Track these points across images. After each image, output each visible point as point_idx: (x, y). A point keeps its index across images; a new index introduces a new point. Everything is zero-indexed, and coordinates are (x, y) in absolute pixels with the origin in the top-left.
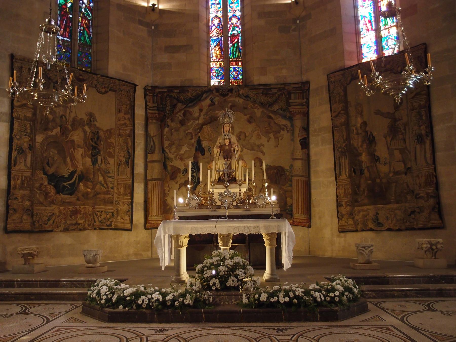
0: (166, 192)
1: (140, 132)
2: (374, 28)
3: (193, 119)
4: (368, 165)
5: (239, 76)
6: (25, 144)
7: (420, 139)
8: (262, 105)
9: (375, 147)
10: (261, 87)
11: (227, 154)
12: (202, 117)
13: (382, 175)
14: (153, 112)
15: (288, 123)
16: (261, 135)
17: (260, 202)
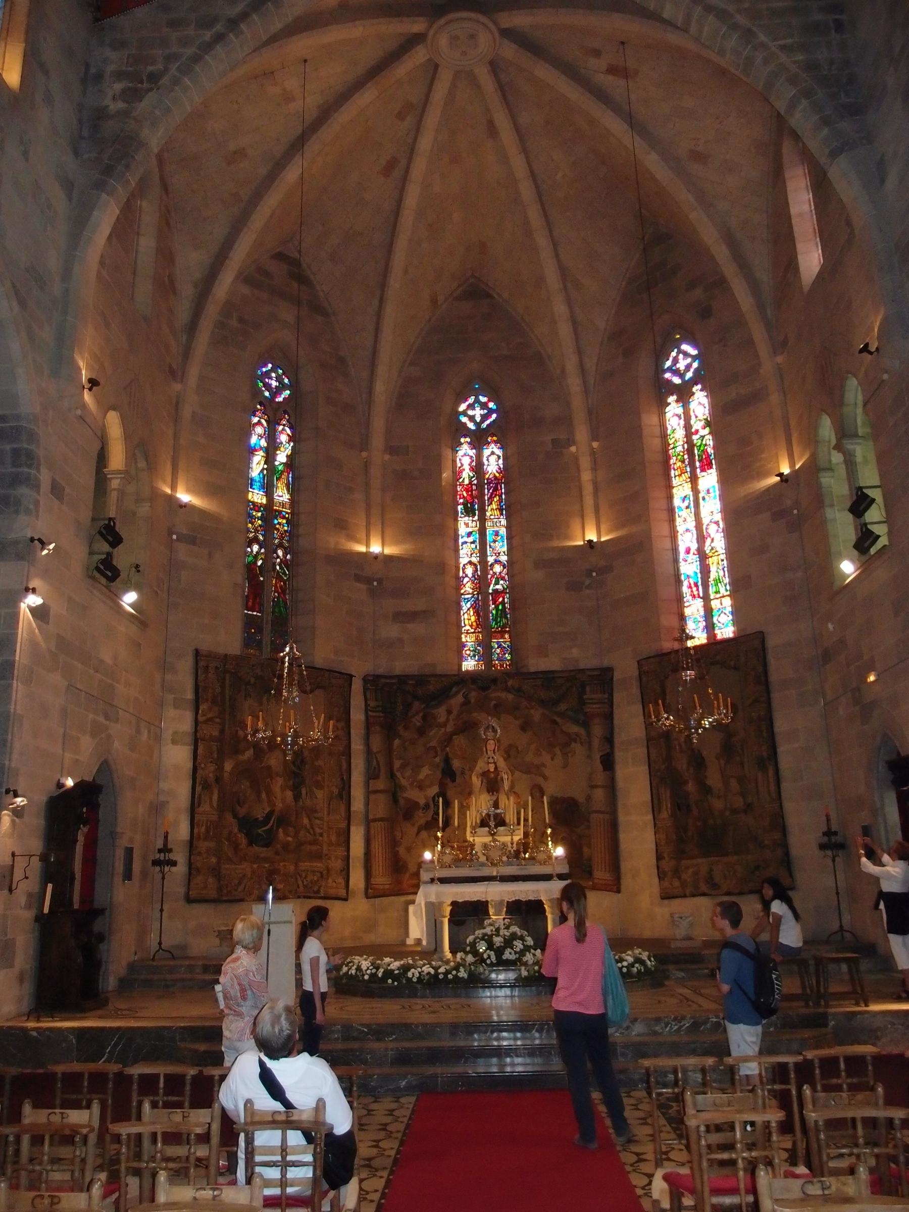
1: (358, 747)
2: (701, 595)
6: (211, 775)
7: (761, 764)
8: (543, 703)
11: (492, 785)
12: (451, 723)
14: (377, 714)
17: (541, 857)
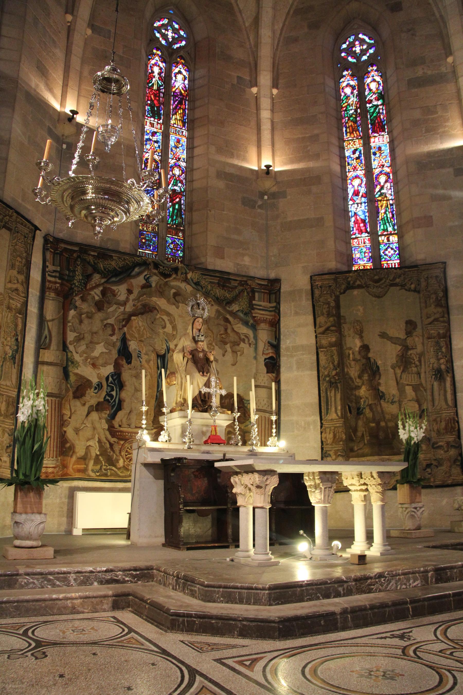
0: (66, 418)
3: (116, 304)
4: (370, 403)
5: (179, 252)
7: (439, 375)
8: (218, 301)
9: (379, 379)
10: (217, 275)
13: (387, 417)
15: (250, 333)
16: (214, 344)
